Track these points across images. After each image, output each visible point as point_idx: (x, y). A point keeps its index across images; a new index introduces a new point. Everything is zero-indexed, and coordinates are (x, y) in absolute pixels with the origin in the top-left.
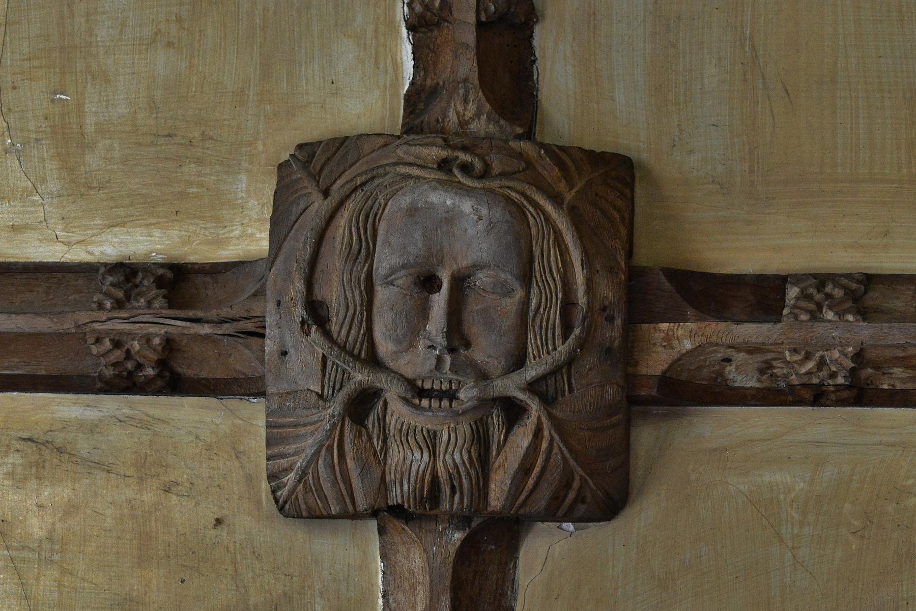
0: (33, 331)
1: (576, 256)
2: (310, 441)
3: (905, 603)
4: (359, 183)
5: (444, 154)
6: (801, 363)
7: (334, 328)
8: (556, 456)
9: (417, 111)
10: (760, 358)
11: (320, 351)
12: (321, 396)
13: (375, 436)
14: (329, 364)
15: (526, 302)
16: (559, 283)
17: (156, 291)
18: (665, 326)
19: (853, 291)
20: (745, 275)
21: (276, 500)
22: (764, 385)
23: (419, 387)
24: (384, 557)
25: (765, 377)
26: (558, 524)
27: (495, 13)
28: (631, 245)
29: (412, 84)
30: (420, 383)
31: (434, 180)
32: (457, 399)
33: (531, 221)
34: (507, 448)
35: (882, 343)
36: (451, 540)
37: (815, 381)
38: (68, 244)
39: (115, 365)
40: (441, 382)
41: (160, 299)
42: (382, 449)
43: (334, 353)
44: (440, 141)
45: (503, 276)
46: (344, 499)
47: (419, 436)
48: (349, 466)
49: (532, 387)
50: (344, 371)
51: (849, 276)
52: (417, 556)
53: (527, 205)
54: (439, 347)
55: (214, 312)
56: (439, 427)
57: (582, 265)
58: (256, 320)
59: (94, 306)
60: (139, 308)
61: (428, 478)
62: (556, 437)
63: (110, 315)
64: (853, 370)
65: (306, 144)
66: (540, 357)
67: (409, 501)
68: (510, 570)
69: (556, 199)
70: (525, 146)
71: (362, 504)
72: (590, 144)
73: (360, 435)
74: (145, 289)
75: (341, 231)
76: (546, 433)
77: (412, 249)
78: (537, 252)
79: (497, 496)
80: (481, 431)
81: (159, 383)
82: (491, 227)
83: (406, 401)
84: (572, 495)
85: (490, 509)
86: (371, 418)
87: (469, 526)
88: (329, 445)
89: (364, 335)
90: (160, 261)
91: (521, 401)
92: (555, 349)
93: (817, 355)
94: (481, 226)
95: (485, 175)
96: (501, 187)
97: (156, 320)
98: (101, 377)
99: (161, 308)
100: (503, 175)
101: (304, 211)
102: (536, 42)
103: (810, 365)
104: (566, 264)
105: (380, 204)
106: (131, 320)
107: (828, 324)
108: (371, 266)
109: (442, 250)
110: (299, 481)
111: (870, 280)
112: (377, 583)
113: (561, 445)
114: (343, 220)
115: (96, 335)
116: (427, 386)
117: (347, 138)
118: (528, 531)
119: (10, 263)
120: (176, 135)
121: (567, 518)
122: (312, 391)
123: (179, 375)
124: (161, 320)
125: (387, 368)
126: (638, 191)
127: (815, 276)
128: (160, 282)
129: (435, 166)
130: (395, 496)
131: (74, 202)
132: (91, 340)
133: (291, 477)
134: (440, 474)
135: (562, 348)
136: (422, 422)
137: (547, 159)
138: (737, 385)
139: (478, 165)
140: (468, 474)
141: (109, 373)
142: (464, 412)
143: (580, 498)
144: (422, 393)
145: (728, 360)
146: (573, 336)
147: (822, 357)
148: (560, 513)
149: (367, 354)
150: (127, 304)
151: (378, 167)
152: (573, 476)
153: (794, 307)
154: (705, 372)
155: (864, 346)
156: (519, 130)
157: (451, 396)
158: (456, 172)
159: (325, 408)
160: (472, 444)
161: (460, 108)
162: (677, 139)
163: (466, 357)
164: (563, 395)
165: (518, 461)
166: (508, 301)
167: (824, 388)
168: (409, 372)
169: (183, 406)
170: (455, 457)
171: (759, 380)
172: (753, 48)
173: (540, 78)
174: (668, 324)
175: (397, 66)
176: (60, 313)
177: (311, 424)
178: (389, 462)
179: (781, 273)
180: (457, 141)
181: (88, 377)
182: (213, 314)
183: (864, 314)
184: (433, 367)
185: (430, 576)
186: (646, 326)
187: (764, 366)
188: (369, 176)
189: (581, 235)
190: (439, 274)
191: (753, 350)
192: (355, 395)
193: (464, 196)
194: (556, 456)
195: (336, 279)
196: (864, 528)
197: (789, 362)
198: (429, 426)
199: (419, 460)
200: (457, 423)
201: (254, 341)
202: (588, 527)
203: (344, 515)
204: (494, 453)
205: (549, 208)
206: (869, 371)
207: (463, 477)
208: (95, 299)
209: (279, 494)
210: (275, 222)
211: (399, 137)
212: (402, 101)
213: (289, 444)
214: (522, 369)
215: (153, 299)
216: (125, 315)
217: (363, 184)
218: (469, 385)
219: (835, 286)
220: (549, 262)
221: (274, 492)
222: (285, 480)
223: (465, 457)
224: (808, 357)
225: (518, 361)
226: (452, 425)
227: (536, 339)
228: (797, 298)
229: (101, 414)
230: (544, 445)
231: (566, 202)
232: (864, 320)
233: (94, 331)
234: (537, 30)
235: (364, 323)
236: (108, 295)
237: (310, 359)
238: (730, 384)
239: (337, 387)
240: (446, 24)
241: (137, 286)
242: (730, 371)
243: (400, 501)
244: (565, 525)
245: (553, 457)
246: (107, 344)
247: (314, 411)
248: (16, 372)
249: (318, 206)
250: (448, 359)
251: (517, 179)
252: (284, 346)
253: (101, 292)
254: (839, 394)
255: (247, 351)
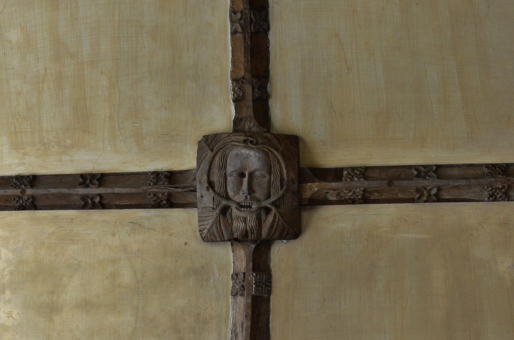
0: (131, 192)
1: (283, 166)
2: (211, 221)
3: (380, 259)
4: (221, 147)
5: (245, 138)
6: (348, 193)
7: (216, 189)
8: (280, 223)
9: (237, 125)
10: (337, 192)
11: (212, 196)
12: (213, 208)
13: (229, 219)
14: (215, 199)
15: (270, 179)
16: (279, 174)
17: (165, 179)
18: (309, 184)
19: (362, 172)
20: (331, 168)
21: (202, 237)
22: (339, 199)
23: (240, 205)
24: (233, 252)
25: (338, 197)
26: (282, 241)
27: (258, 97)
28: (299, 161)
29: (235, 117)
30: (241, 204)
31: (242, 146)
32: (252, 208)
33: (270, 156)
34: (266, 221)
35: (371, 186)
36: (251, 247)
37: (353, 198)
38: (139, 166)
39: (154, 201)
40: (247, 203)
41: (166, 182)
42: (231, 223)
43: (216, 196)
44: (243, 134)
45: (263, 172)
46: (221, 236)
47: (241, 218)
48: (222, 228)
49: (273, 204)
50: (219, 201)
51: (361, 167)
52: (242, 252)
53: (269, 152)
54: (246, 193)
55: (182, 185)
56: (247, 216)
57: (285, 169)
58: (194, 187)
59: (148, 185)
60: (161, 185)
61: (244, 230)
62: (280, 217)
63: (153, 187)
64: (363, 195)
65: (206, 136)
66: (275, 195)
67: (239, 237)
68: (268, 254)
69: (277, 150)
70: (268, 135)
71: (226, 238)
72: (286, 132)
73: (225, 219)
74: (162, 179)
75: (217, 161)
76: (277, 216)
77: (237, 166)
78: (272, 165)
79: (264, 234)
80: (259, 217)
81: (167, 205)
82: (259, 158)
83: (237, 209)
84: (285, 233)
85: (262, 238)
86: (228, 214)
87: (257, 243)
88: (216, 222)
89: (225, 191)
90: (166, 170)
91: (270, 208)
92: (279, 192)
93: (353, 190)
94: (256, 159)
95: (257, 144)
96: (261, 147)
97: (165, 188)
98: (151, 204)
99: (167, 184)
100: (262, 143)
101: (206, 156)
102: (269, 104)
103: (351, 193)
104: (281, 168)
105: (227, 153)
106: (158, 188)
107: (355, 182)
108: (226, 171)
109: (245, 166)
110: (208, 232)
111: (367, 168)
112: (231, 259)
113: (282, 219)
114: (217, 158)
115: (149, 193)
116: (243, 204)
117: (217, 134)
118: (273, 243)
119: (123, 173)
120: (169, 134)
121: (284, 239)
122: (211, 207)
123: (173, 203)
124: (167, 188)
125: (232, 200)
126: (300, 146)
127: (351, 168)
128: (166, 177)
129: (243, 142)
130: (235, 236)
131: (141, 154)
132: (147, 195)
133: (206, 231)
134: (248, 229)
135: (280, 192)
136: (242, 215)
137: (274, 138)
138: (330, 199)
139: (255, 141)
140: (256, 228)
141: (153, 203)
142: (254, 211)
143: (288, 234)
144: (242, 206)
145: (328, 193)
146: (283, 189)
147: (354, 191)
148: (282, 238)
149: (226, 196)
150: (157, 184)
151: (226, 143)
152: (285, 228)
153: (346, 177)
154: (321, 196)
155: (366, 187)
156: (266, 130)
157: (250, 207)
158: (248, 143)
159: (214, 212)
160: (256, 220)
161: (249, 124)
162: (310, 130)
163: (254, 196)
164: (281, 205)
165: (270, 225)
166: (265, 179)
167: (355, 200)
168: (238, 201)
169: (174, 211)
170: (252, 224)
171: (336, 198)
172: (331, 103)
173: (271, 115)
174: (310, 184)
175: (230, 112)
176: (138, 187)
177: (210, 216)
178: (233, 226)
179: (342, 167)
180: (248, 134)
181: (147, 204)
182: (182, 185)
183: (366, 178)
184: (245, 199)
185: (246, 258)
186: (304, 184)
187: (338, 194)
188: (224, 146)
189: (284, 159)
190: (245, 172)
191: (334, 190)
192: (223, 207)
193: (251, 150)
194: (280, 223)
195: (216, 175)
196: (368, 238)
197: (345, 193)
198: (244, 216)
199: (242, 225)
200: (252, 215)
201: (193, 193)
202: (290, 241)
203: (221, 241)
204: (263, 223)
205: (275, 153)
206: (368, 194)
207: (254, 229)
208: (148, 183)
209: (202, 235)
210: (198, 159)
211: (232, 134)
212: (232, 122)
213: (205, 222)
214: (270, 198)
215: (164, 182)
216: (157, 187)
217: (222, 148)
218: (255, 204)
219: (357, 171)
220: (276, 168)
221: (201, 235)
222: (204, 232)
223: (255, 224)
224: (350, 191)
225: (268, 196)
226: (251, 215)
227: (273, 190)
228: (346, 175)
229: (151, 214)
230: (277, 220)
231: (280, 150)
232: (366, 180)
233: (148, 192)
234: (270, 100)
235: (224, 187)
236: (151, 181)
237: (209, 198)
238: (328, 199)
239: (218, 205)
240: (244, 100)
241: (159, 178)
242: (328, 196)
243: (237, 237)
244: (283, 241)
245: (280, 223)
246: (152, 195)
247: (211, 213)
248: (126, 204)
249: (210, 154)
250: (249, 197)
251: (266, 145)
252: (202, 194)
253: (150, 181)
254: (359, 201)
255: (192, 196)
